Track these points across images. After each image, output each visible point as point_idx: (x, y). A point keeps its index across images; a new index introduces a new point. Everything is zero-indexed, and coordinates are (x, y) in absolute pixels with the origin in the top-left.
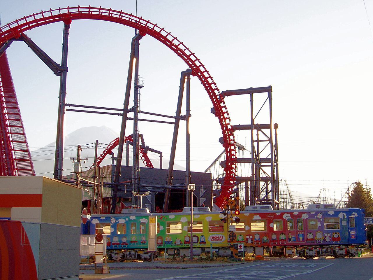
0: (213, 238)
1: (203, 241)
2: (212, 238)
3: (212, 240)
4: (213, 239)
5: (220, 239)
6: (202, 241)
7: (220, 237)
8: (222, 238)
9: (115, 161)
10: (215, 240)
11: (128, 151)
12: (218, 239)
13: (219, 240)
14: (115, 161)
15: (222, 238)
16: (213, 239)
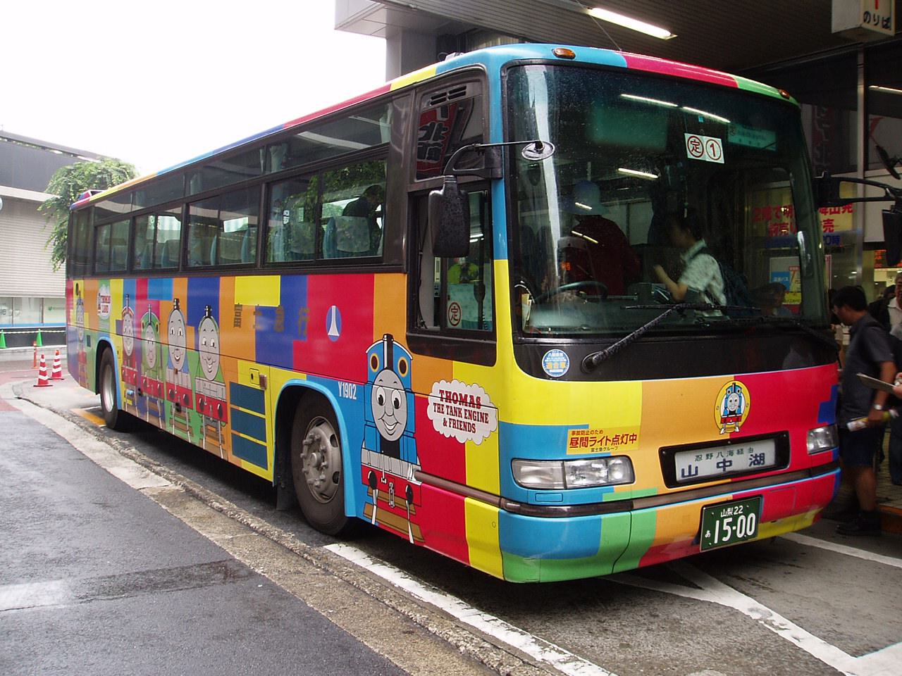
6: (731, 413)
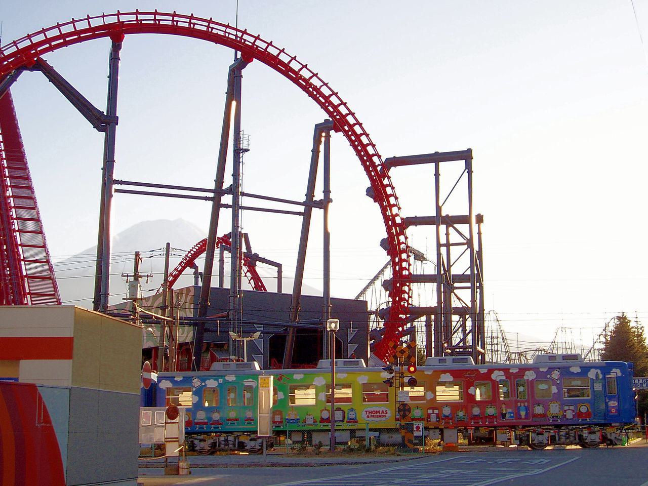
0: (369, 413)
1: (353, 419)
2: (368, 412)
3: (368, 417)
4: (370, 415)
5: (383, 414)
6: (351, 419)
7: (383, 411)
8: (385, 413)
9: (200, 279)
10: (373, 416)
11: (222, 261)
12: (378, 414)
13: (380, 416)
14: (200, 279)
15: (385, 413)
16: (370, 415)
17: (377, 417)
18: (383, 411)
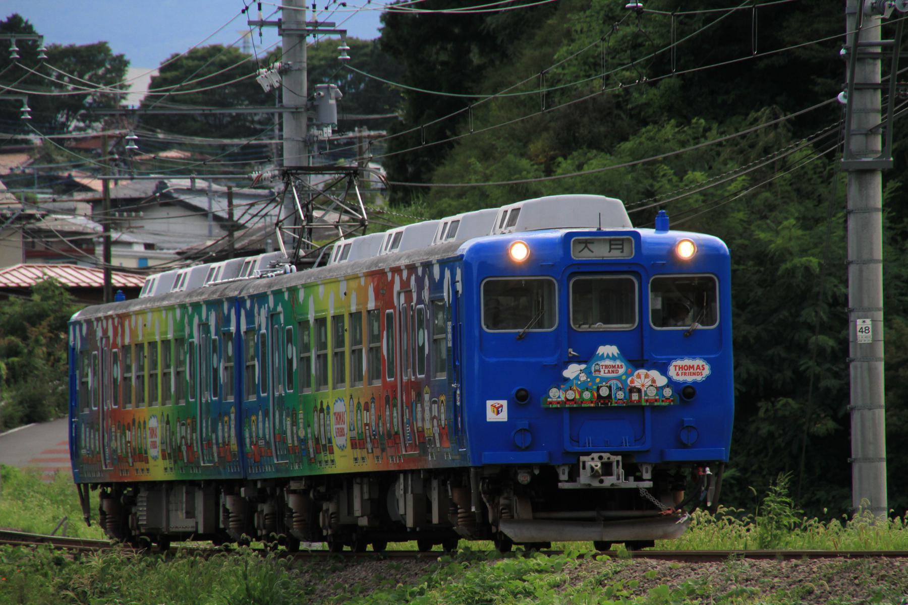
0: (679, 368)
2: (677, 368)
3: (678, 375)
4: (680, 372)
7: (698, 366)
9: (442, 408)
10: (685, 374)
12: (692, 370)
13: (694, 374)
14: (442, 408)
16: (680, 372)
17: (690, 374)
18: (698, 366)
